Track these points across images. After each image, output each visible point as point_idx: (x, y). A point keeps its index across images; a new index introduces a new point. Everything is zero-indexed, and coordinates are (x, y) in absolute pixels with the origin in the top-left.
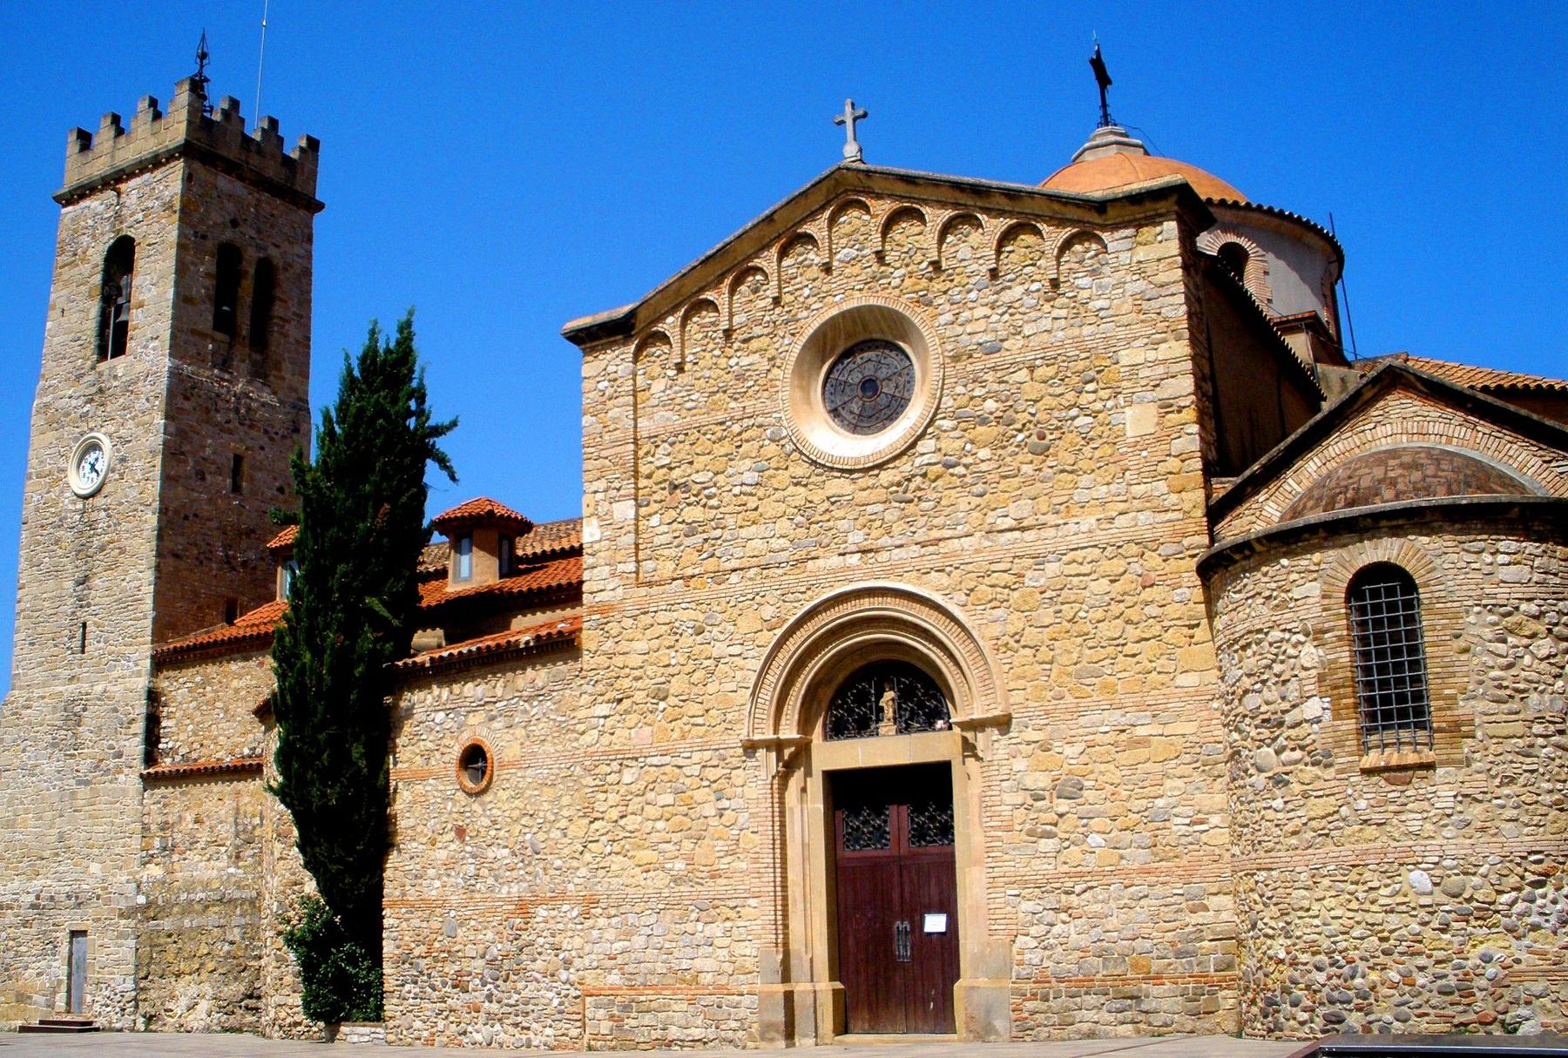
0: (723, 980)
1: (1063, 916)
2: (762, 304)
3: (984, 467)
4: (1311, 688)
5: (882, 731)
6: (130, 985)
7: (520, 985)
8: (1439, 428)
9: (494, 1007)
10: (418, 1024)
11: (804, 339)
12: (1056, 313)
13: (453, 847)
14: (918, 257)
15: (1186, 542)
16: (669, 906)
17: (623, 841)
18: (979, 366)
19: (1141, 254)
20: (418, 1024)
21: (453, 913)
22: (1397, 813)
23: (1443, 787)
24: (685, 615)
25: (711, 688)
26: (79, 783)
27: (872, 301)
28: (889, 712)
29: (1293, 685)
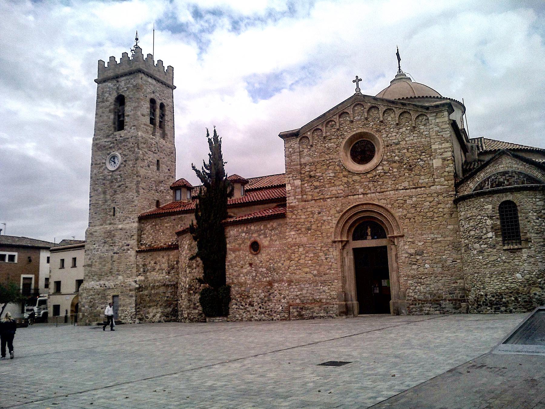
0: (328, 301)
1: (419, 284)
2: (334, 130)
3: (395, 174)
6: (134, 310)
7: (270, 304)
8: (516, 166)
9: (262, 310)
10: (238, 316)
11: (345, 140)
13: (248, 268)
14: (377, 120)
16: (313, 282)
17: (299, 266)
18: (394, 148)
19: (438, 120)
20: (238, 316)
23: (525, 254)
25: (323, 227)
26: (114, 253)
27: (365, 131)
29: (485, 229)
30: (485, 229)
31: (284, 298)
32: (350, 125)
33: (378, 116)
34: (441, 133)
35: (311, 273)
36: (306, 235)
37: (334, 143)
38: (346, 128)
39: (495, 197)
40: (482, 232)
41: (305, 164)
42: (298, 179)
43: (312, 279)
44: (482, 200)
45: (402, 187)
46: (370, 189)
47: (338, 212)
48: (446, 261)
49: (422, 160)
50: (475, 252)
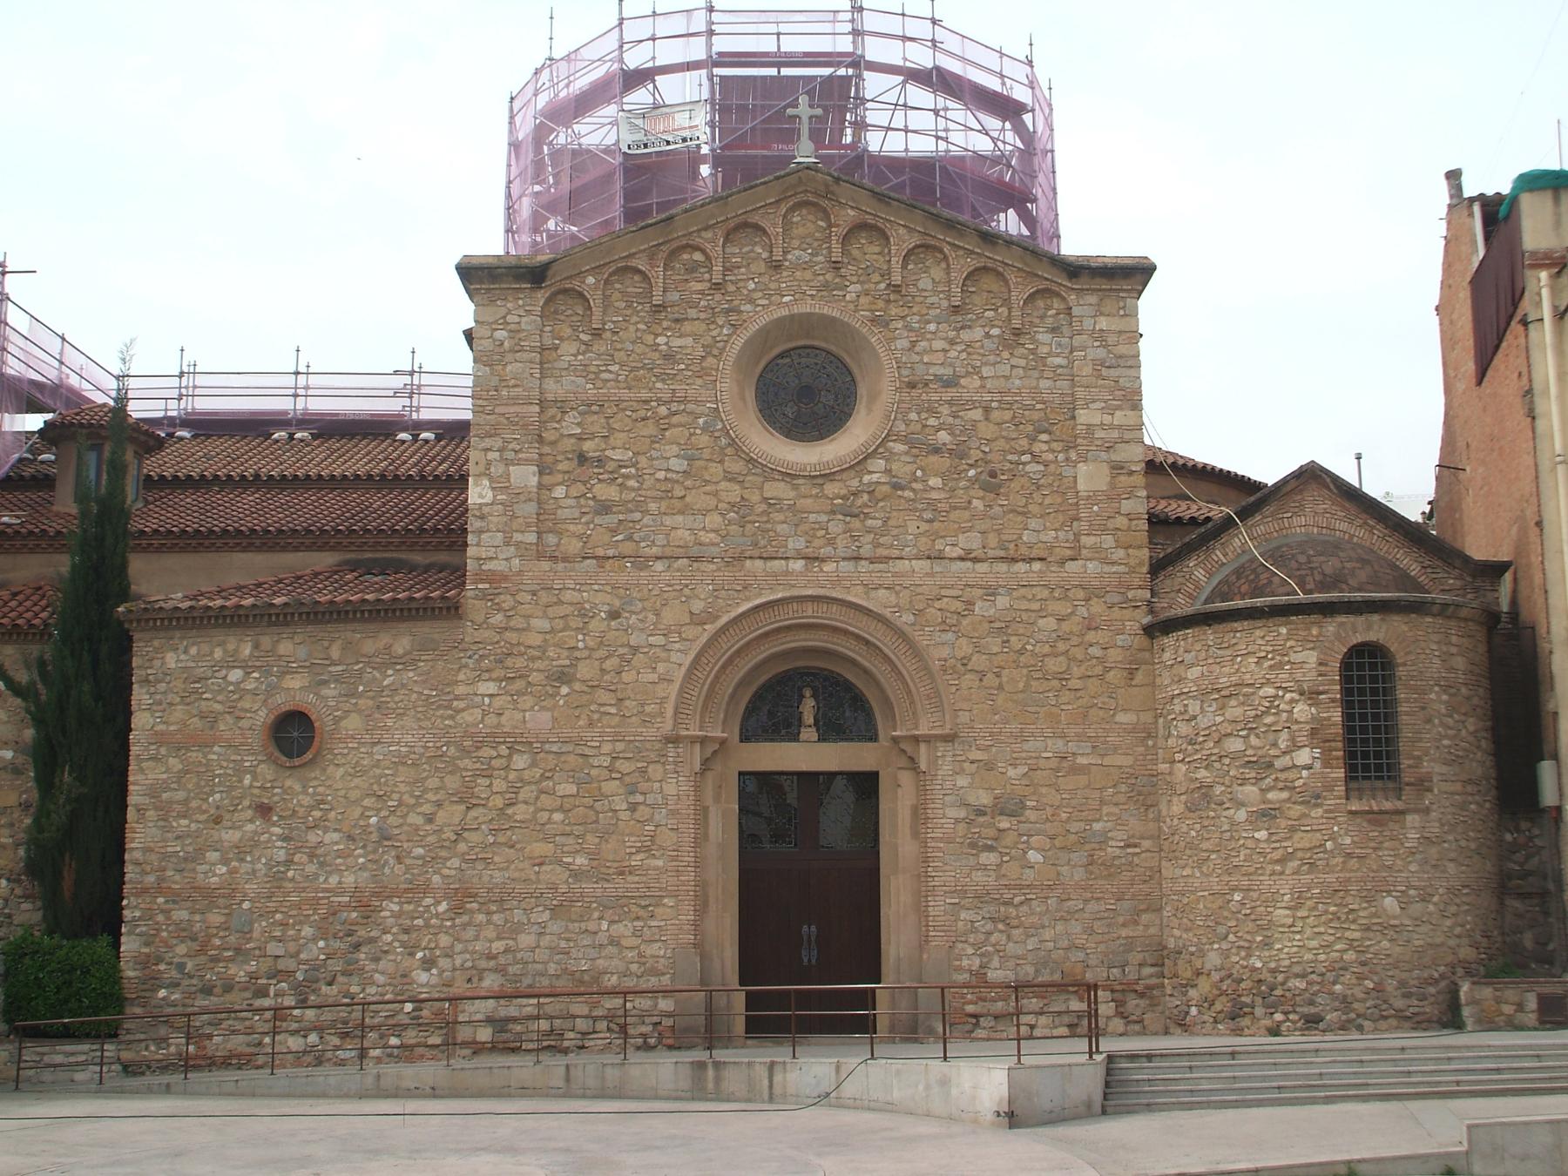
2: (699, 286)
3: (934, 495)
4: (1302, 740)
5: (803, 736)
12: (1014, 361)
13: (250, 827)
15: (1130, 595)
18: (935, 397)
19: (1103, 323)
21: (246, 905)
22: (1375, 849)
24: (600, 597)
25: (626, 677)
28: (809, 718)
29: (1285, 735)
30: (1285, 735)
31: (428, 964)
32: (765, 279)
33: (880, 262)
34: (1113, 373)
35: (560, 862)
36: (548, 703)
37: (697, 337)
38: (752, 286)
39: (1331, 626)
40: (1275, 745)
41: (563, 406)
42: (527, 462)
43: (563, 888)
44: (1284, 630)
45: (957, 552)
46: (831, 542)
47: (697, 620)
48: (1104, 840)
49: (1035, 458)
50: (1241, 815)
